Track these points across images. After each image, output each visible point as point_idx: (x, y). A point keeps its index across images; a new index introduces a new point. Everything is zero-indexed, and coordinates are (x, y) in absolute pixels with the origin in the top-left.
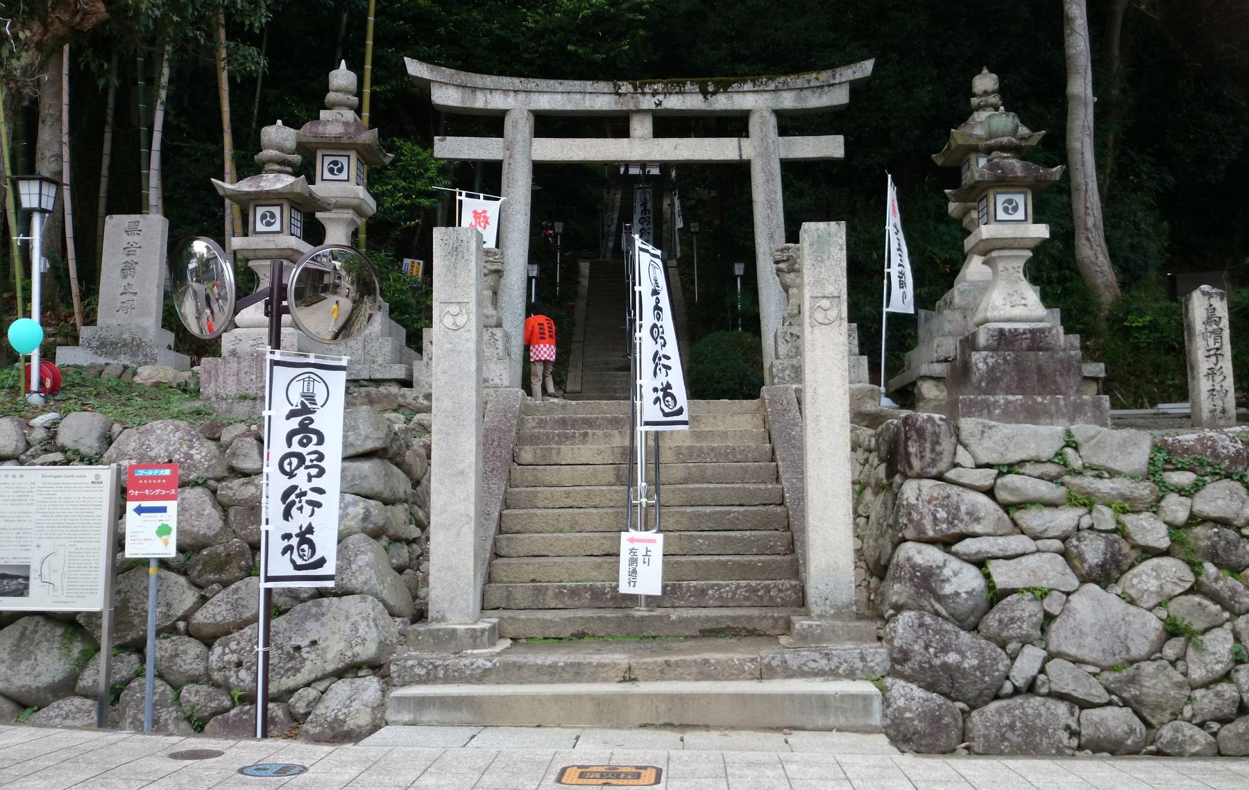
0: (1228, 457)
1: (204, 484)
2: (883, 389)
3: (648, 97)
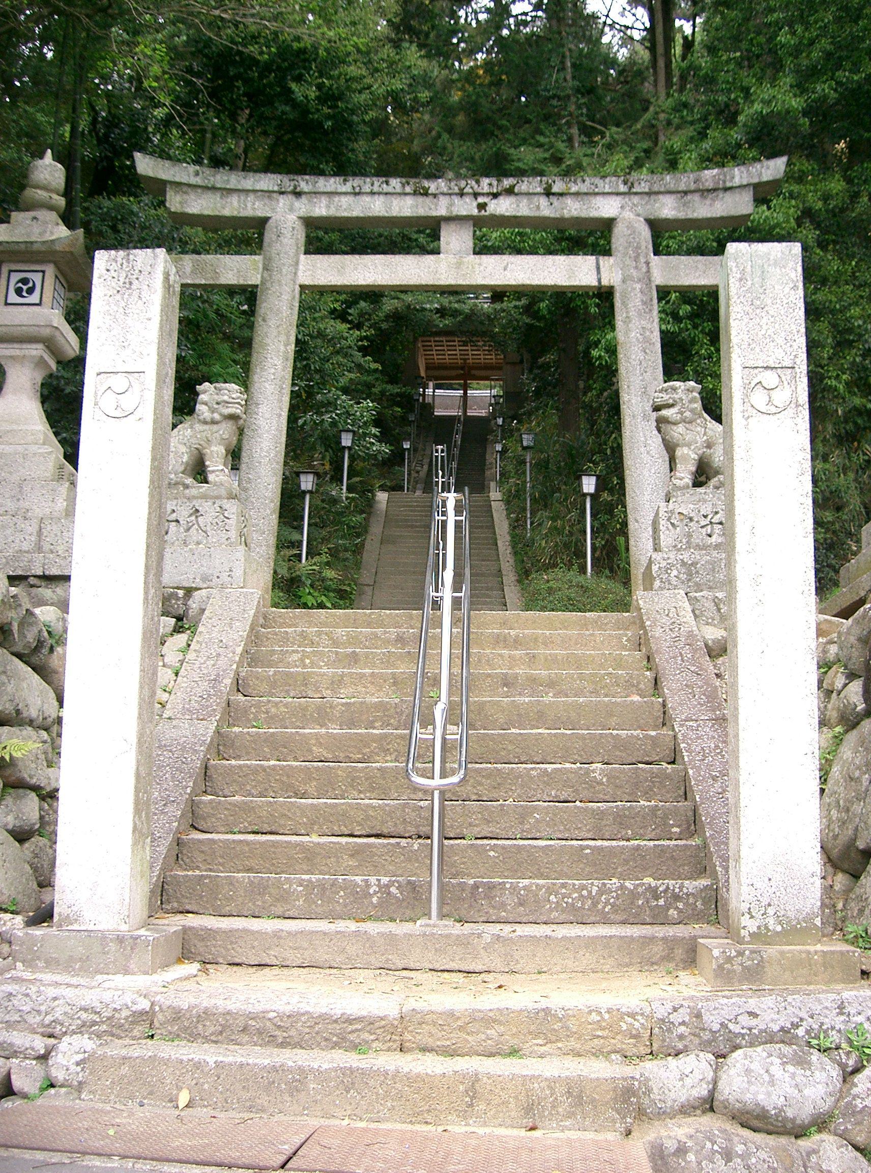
3: (467, 199)
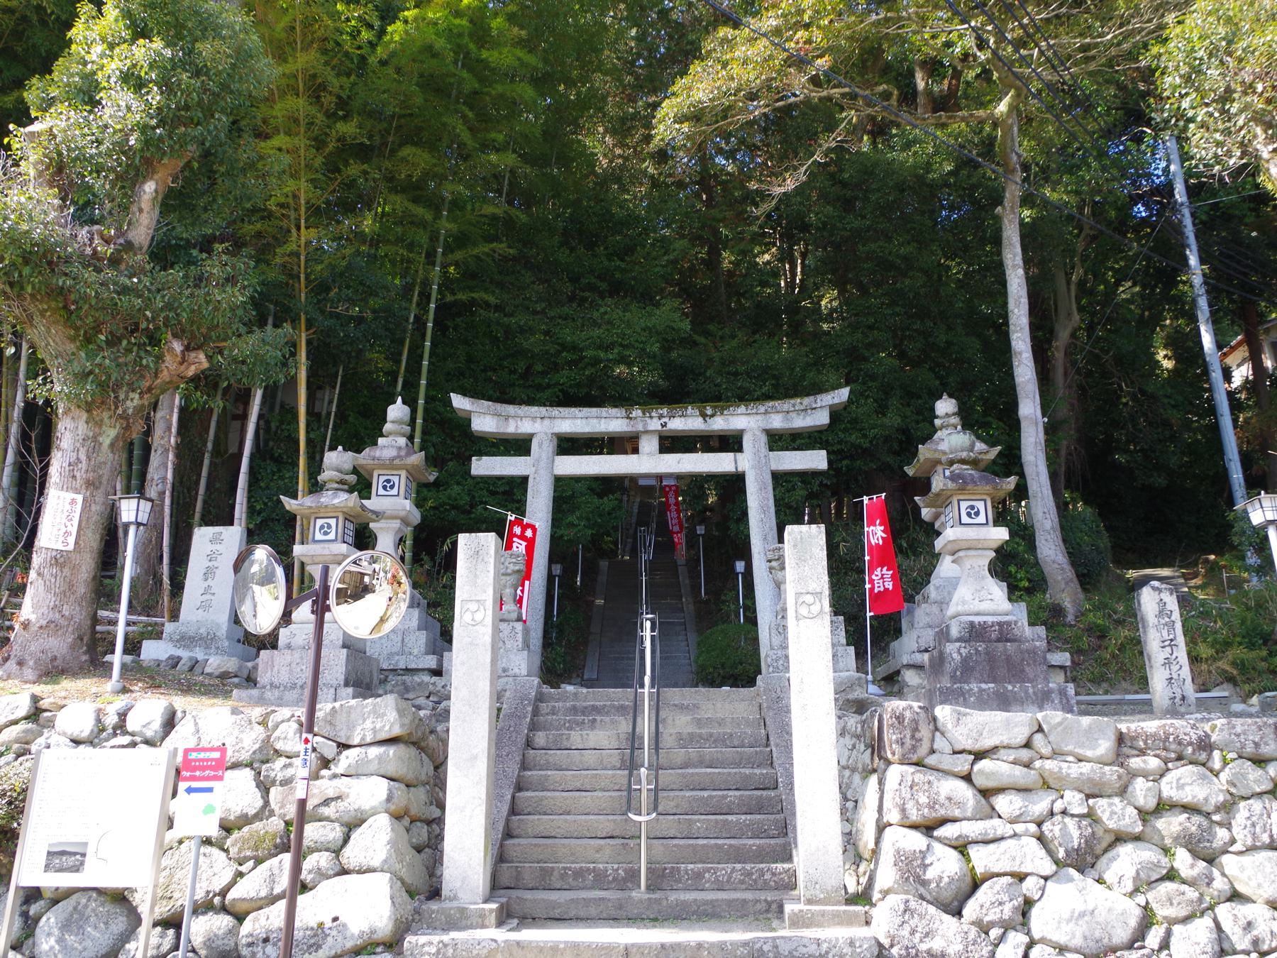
0: (1190, 744)
1: (250, 765)
2: (870, 677)
3: (655, 420)
